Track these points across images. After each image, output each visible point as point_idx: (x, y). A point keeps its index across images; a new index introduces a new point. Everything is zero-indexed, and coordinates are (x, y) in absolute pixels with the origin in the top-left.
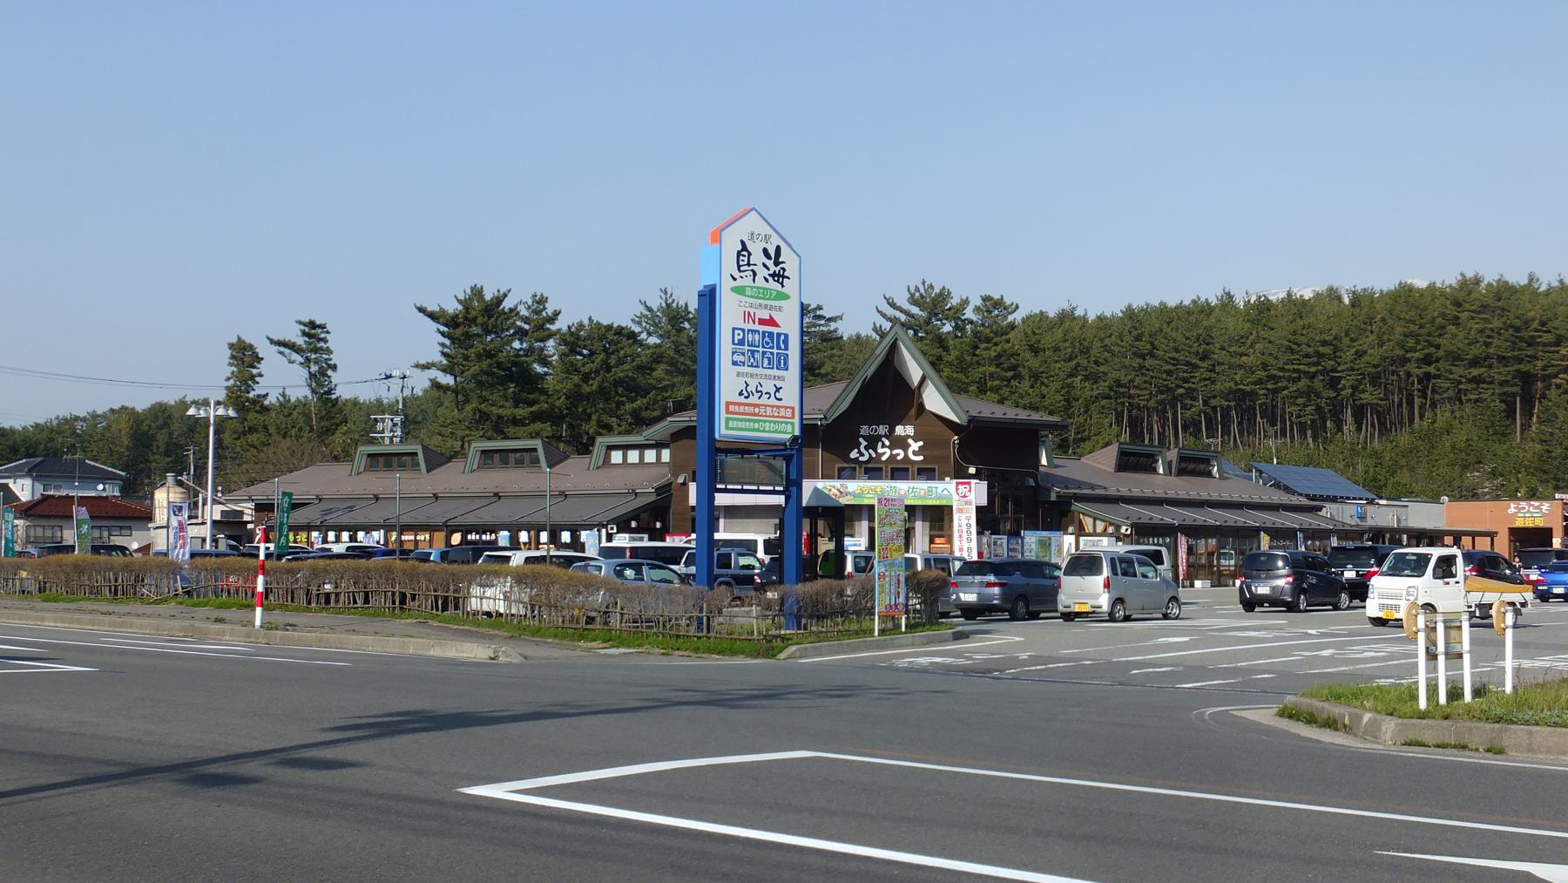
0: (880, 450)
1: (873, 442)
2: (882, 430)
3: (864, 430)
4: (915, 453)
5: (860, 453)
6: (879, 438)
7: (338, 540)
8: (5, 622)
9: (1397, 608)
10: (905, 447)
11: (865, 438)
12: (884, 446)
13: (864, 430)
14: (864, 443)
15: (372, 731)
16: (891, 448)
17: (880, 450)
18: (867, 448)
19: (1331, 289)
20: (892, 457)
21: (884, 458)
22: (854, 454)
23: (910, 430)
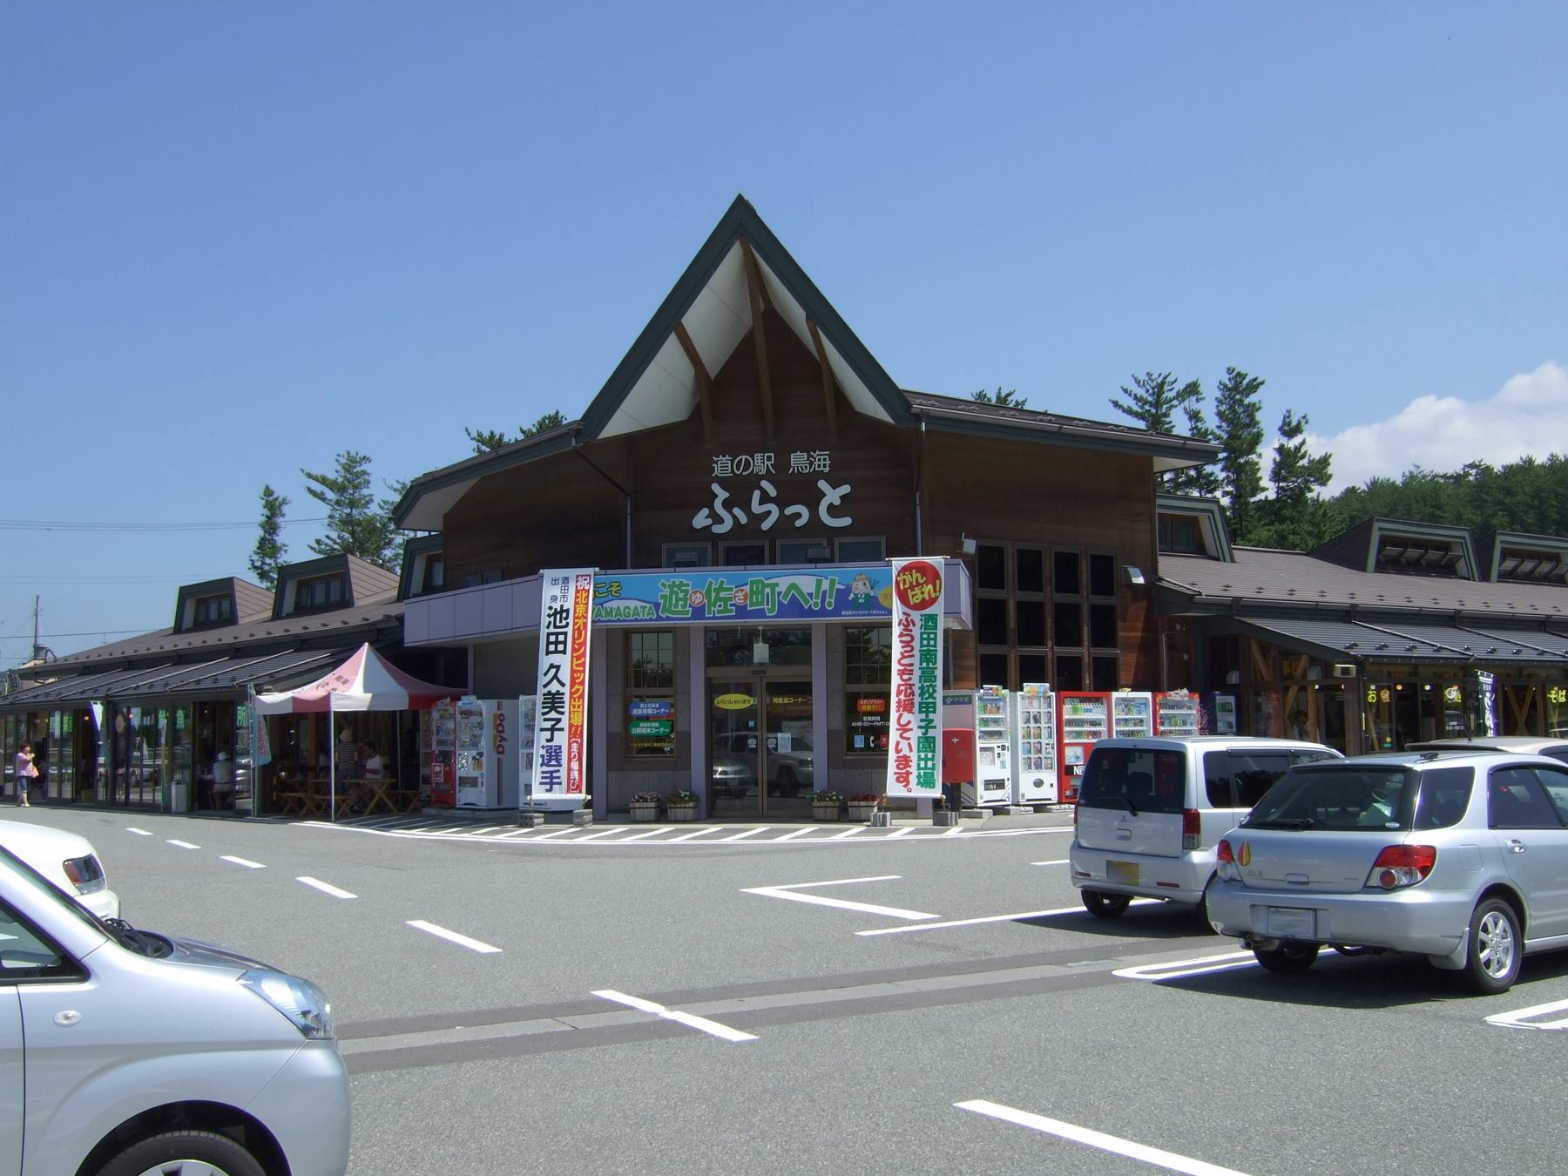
0: (757, 508)
1: (740, 491)
2: (761, 463)
3: (723, 465)
4: (832, 510)
5: (717, 517)
6: (753, 482)
7: (1225, 494)
8: (1555, 648)
9: (903, 779)
10: (813, 499)
11: (724, 483)
12: (765, 498)
13: (723, 465)
14: (722, 495)
15: (322, 656)
16: (782, 502)
17: (757, 508)
18: (727, 505)
19: (185, 593)
20: (786, 522)
21: (766, 526)
22: (701, 520)
23: (822, 461)
